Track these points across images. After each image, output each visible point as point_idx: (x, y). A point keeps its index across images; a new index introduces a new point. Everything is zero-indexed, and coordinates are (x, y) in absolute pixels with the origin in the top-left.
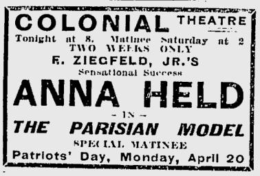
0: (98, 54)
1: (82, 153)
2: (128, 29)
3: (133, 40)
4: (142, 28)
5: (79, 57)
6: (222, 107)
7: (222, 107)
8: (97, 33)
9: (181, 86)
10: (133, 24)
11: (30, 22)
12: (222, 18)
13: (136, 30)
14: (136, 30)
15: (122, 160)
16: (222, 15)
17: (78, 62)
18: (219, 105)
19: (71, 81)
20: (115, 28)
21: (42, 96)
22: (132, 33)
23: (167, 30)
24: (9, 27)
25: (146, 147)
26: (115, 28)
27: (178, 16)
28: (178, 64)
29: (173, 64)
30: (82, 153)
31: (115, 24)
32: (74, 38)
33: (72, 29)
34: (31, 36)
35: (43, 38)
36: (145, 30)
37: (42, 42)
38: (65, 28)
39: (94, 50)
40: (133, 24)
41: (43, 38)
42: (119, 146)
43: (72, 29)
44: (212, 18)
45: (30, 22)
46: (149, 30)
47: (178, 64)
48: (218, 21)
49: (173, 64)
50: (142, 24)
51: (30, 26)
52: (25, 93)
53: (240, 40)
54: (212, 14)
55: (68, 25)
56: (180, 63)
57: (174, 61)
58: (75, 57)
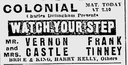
1: (17, 49)
2: (57, 10)
3: (57, 16)
4: (64, 10)
8: (43, 12)
10: (60, 8)
11: (10, 9)
13: (62, 11)
14: (62, 11)
15: (52, 38)
19: (9, 36)
20: (51, 10)
21: (18, 36)
22: (60, 13)
23: (76, 11)
25: (117, 6)
26: (51, 10)
28: (15, 43)
29: (13, 43)
30: (17, 49)
31: (51, 8)
33: (30, 11)
34: (92, 14)
35: (63, 15)
36: (66, 11)
38: (27, 11)
40: (60, 8)
41: (63, 15)
43: (30, 11)
45: (10, 9)
46: (67, 11)
47: (15, 43)
49: (13, 43)
50: (64, 8)
51: (10, 11)
53: (102, 9)
55: (28, 9)
56: (16, 42)
57: (13, 42)
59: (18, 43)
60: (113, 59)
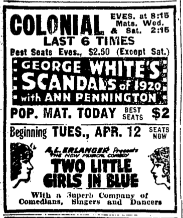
0: (51, 199)
5: (136, 135)
6: (37, 34)
7: (37, 34)
9: (143, 78)
12: (164, 128)
16: (163, 126)
17: (138, 134)
18: (45, 36)
24: (161, 209)
27: (128, 128)
32: (145, 15)
34: (115, 205)
37: (87, 204)
39: (100, 194)
42: (65, 117)
44: (159, 128)
48: (162, 130)
52: (99, 132)
54: (160, 126)
58: (139, 136)
59: (70, 117)
60: (93, 202)
